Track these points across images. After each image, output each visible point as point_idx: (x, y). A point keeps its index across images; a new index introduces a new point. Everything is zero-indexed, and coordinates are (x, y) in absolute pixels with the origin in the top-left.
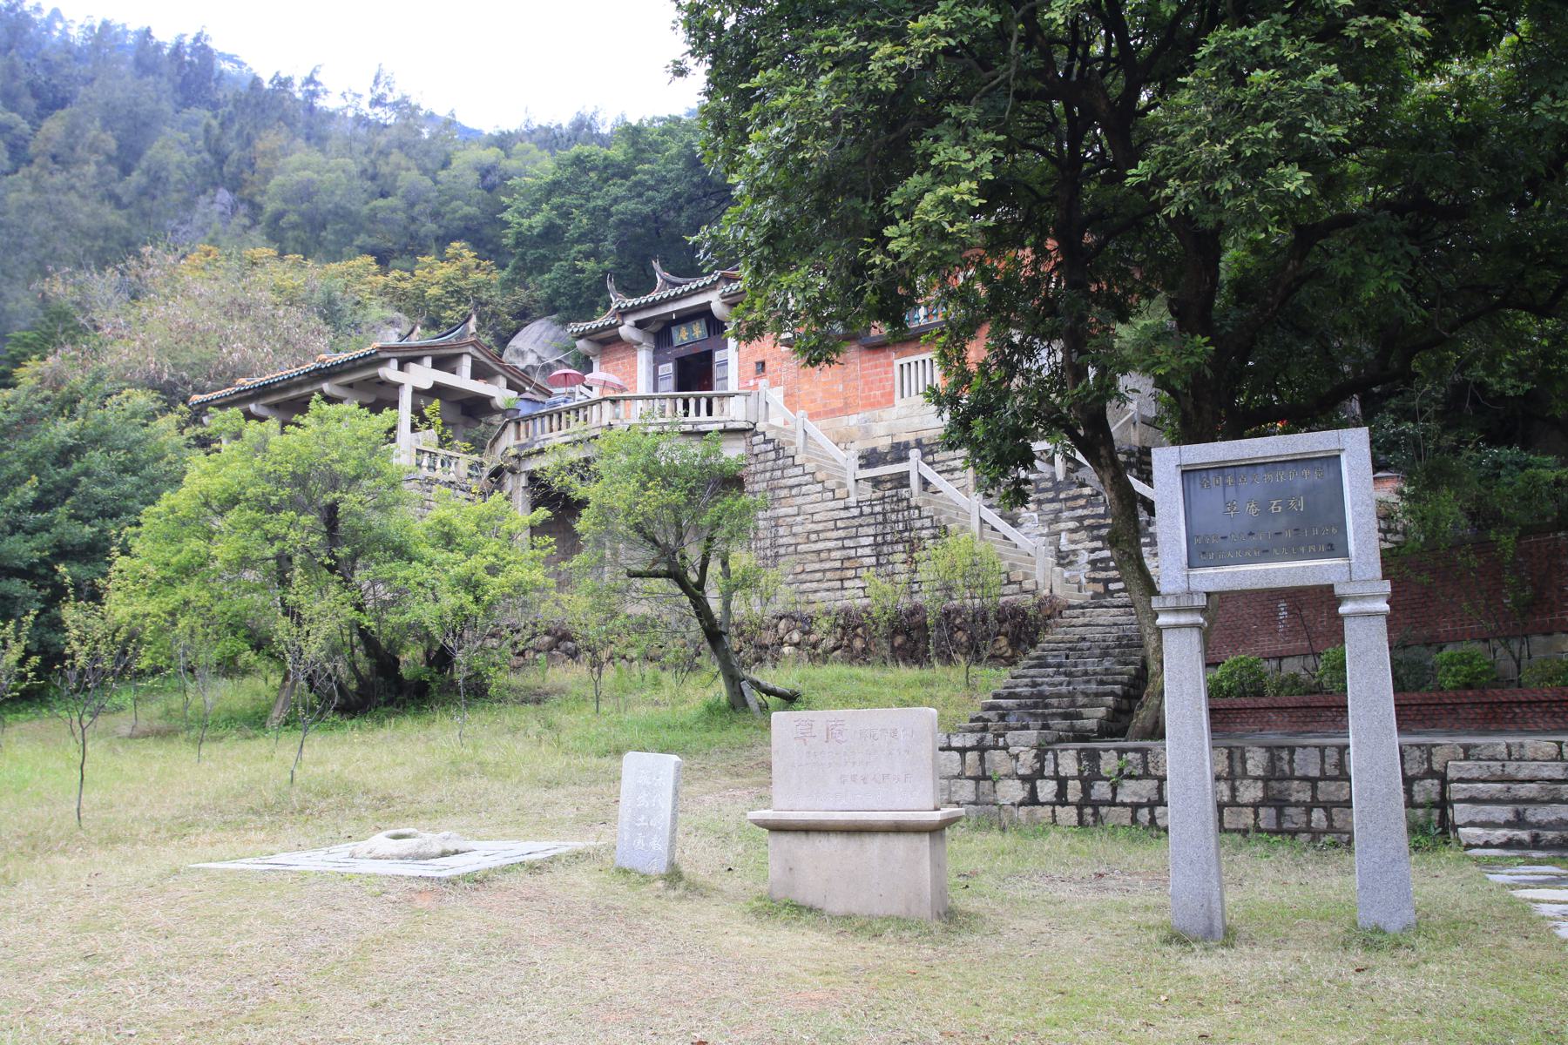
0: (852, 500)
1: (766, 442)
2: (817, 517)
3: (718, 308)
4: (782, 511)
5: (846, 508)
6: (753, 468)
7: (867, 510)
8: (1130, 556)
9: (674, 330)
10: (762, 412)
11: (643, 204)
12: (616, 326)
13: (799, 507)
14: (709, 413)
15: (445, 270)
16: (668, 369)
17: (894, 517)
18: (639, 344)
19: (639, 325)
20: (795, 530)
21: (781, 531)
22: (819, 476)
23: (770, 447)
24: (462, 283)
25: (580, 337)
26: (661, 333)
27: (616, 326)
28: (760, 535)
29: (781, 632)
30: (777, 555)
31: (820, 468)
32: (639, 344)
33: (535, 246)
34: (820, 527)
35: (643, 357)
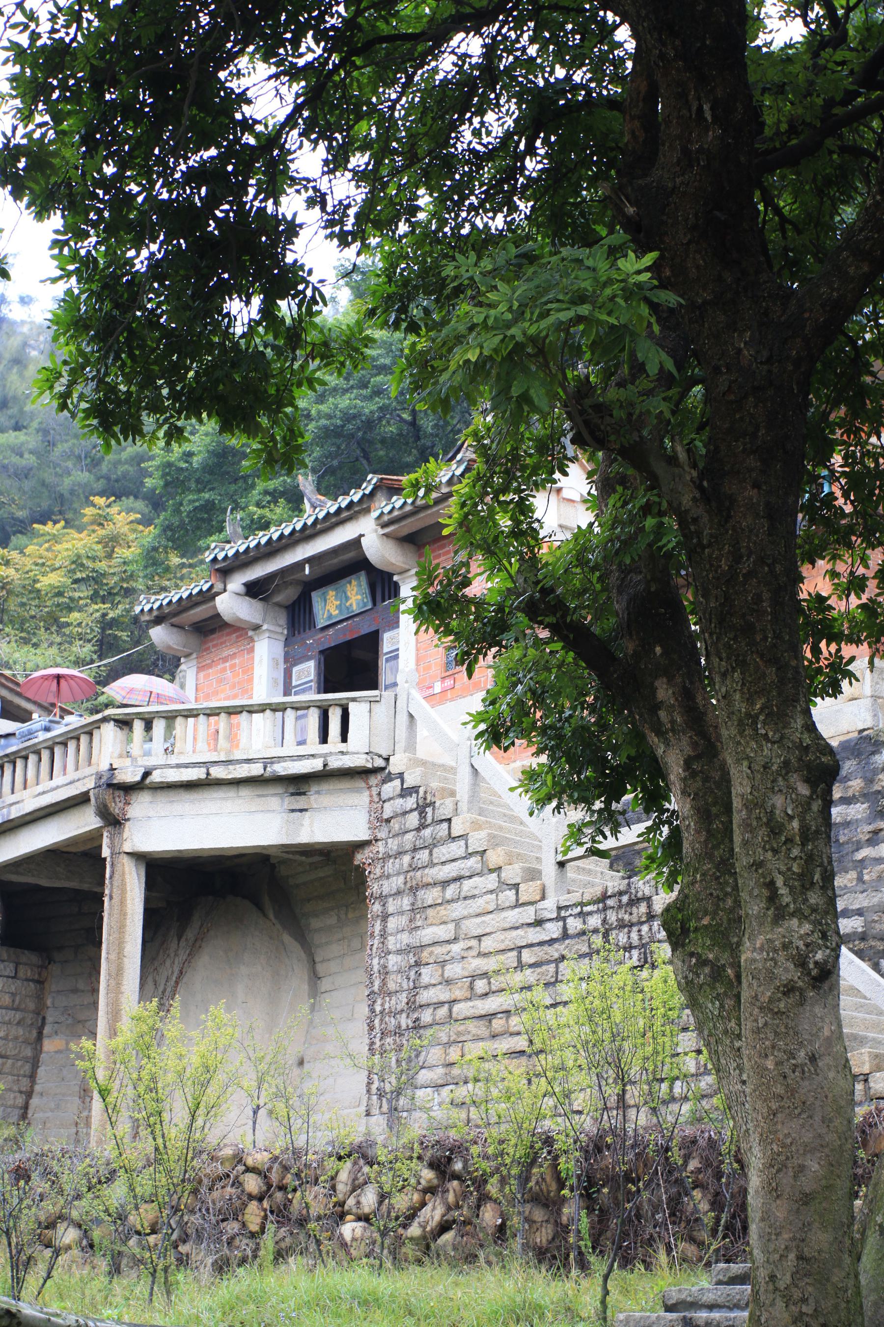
0: (548, 907)
1: (406, 792)
2: (488, 944)
3: (376, 546)
4: (428, 934)
5: (539, 923)
6: (380, 847)
7: (574, 925)
8: (717, 973)
9: (315, 596)
10: (402, 732)
11: (365, 398)
12: (208, 596)
13: (457, 922)
14: (344, 739)
15: (78, 542)
16: (307, 671)
17: (622, 938)
18: (257, 628)
19: (253, 590)
20: (452, 970)
21: (428, 975)
22: (494, 858)
23: (410, 802)
24: (102, 566)
25: (159, 620)
26: (292, 599)
27: (208, 596)
28: (392, 986)
29: (342, 1188)
30: (417, 1026)
31: (495, 841)
32: (257, 628)
33: (202, 485)
34: (490, 965)
35: (266, 651)
